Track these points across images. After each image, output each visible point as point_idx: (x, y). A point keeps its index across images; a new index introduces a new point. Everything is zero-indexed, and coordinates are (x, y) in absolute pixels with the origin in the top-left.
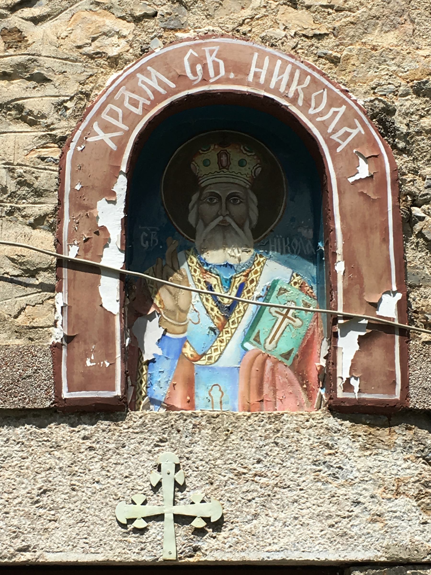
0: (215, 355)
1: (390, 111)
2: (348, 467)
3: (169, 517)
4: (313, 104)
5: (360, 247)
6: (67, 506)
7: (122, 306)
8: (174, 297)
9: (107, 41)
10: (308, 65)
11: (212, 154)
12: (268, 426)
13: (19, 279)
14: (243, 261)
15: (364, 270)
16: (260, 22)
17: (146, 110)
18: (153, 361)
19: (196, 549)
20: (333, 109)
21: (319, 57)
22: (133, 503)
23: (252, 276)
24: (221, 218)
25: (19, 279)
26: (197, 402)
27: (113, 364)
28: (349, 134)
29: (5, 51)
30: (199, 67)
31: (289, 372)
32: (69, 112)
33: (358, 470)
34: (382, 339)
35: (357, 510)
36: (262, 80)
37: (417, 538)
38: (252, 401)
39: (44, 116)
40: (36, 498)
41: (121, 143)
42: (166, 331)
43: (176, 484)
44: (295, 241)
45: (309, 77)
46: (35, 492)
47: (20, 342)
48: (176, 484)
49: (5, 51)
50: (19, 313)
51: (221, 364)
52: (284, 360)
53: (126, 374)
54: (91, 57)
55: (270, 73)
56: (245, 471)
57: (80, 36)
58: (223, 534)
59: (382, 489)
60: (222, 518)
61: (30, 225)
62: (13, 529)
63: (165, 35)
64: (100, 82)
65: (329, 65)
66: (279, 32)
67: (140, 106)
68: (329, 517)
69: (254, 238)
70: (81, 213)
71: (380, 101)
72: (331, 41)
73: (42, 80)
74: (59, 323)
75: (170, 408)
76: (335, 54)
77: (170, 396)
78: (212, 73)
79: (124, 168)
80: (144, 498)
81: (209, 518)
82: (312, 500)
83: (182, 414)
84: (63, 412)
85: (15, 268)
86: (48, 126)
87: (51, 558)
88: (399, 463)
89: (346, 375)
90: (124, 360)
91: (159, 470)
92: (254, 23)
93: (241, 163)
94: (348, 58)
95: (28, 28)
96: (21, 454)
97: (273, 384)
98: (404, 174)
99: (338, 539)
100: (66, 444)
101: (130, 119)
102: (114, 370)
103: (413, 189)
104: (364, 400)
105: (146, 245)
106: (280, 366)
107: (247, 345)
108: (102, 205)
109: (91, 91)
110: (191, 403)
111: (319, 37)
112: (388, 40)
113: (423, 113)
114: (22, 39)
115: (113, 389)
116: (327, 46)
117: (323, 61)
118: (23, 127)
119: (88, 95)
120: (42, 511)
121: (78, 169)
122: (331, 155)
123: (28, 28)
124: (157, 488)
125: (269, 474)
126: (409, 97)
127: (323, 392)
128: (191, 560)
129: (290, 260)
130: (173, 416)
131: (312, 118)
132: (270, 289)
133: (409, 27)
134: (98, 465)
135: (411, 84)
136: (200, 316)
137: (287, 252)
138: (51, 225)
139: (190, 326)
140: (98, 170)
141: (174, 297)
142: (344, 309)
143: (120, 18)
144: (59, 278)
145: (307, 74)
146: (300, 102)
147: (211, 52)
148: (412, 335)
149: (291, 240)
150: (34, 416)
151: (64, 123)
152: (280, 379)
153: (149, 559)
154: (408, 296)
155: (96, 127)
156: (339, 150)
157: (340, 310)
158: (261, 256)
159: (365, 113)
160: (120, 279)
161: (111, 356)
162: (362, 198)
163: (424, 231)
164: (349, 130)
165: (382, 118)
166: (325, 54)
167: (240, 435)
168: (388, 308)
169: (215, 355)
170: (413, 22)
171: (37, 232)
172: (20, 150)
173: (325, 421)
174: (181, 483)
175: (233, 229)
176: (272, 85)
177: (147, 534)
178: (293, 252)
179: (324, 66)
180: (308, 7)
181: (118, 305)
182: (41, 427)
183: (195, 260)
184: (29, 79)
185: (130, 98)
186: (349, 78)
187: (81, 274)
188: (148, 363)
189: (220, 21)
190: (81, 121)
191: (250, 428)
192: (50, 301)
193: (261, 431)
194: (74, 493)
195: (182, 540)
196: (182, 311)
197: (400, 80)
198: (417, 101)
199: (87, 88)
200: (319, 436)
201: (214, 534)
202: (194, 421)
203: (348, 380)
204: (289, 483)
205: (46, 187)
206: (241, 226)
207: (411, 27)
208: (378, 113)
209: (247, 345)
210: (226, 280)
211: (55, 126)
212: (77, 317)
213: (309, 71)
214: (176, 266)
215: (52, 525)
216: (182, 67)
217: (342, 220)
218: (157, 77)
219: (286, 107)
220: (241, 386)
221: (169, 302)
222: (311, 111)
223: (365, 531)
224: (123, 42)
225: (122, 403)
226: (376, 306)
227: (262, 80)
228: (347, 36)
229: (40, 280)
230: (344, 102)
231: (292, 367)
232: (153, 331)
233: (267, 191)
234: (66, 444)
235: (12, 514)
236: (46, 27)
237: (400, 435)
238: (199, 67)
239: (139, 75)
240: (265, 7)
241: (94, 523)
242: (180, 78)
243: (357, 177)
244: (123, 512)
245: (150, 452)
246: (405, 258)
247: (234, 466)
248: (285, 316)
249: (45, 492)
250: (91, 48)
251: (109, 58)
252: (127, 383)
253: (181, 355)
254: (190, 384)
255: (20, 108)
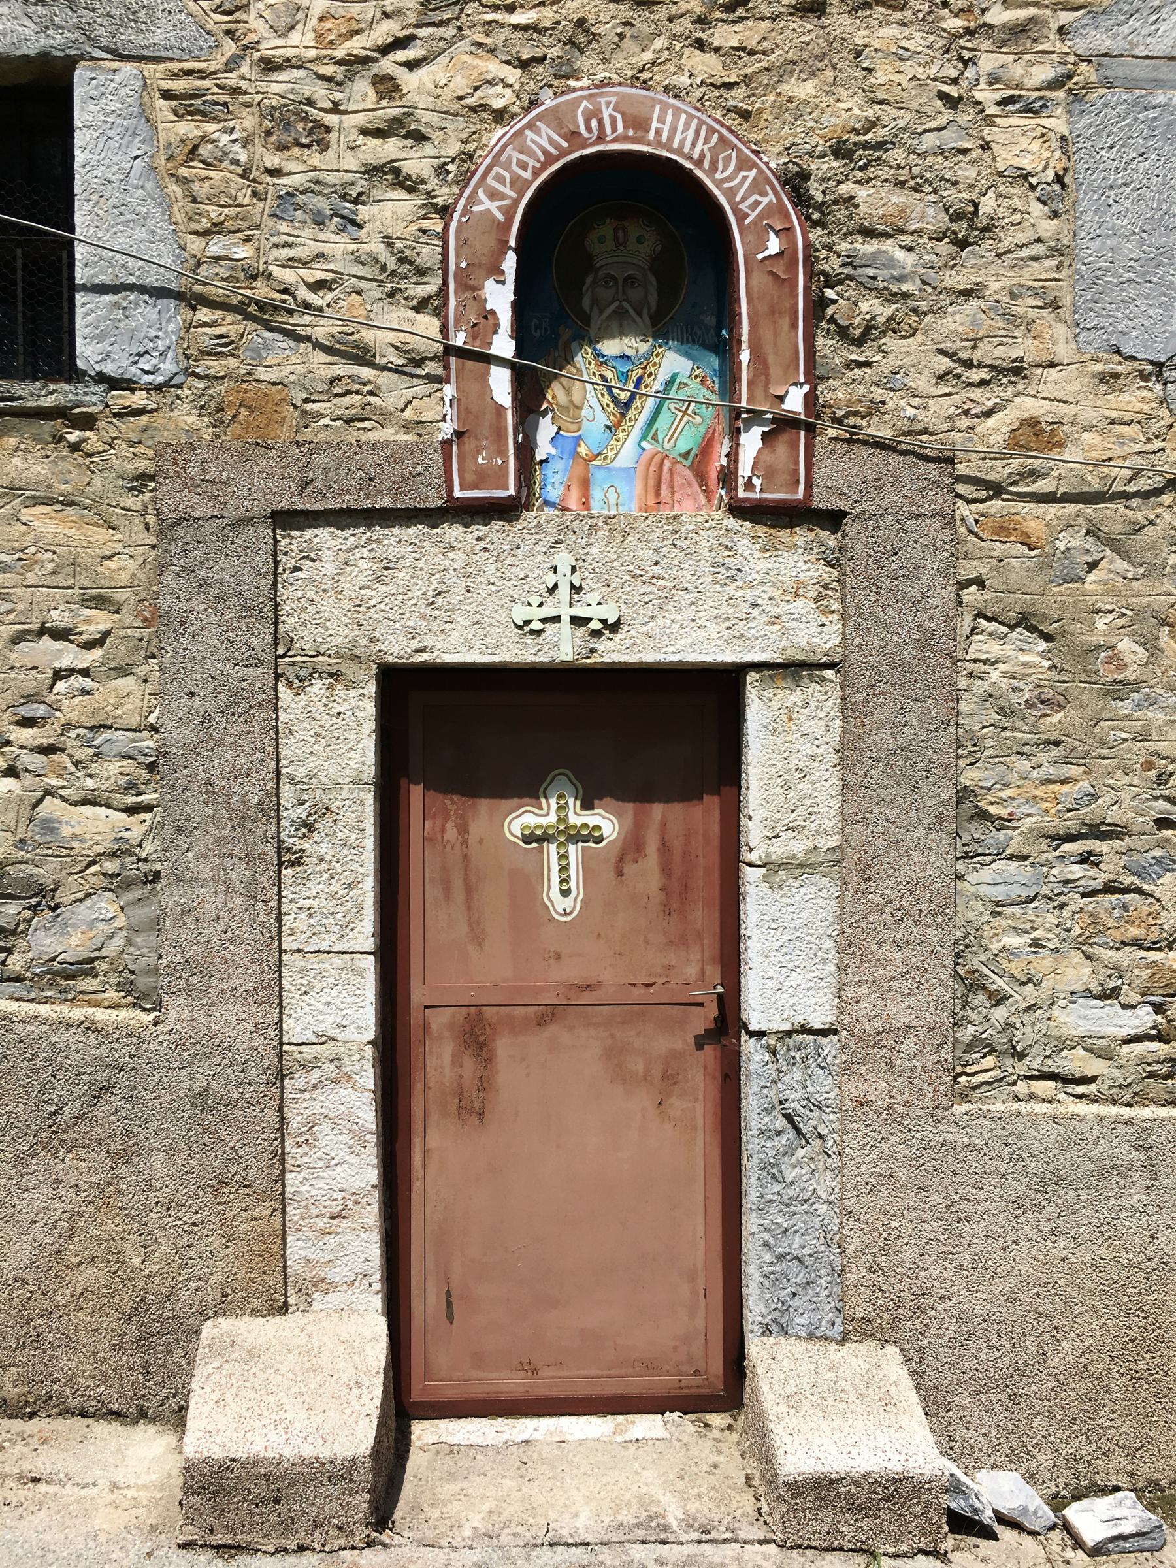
0: (611, 454)
1: (804, 176)
2: (747, 569)
3: (565, 619)
4: (720, 168)
5: (767, 335)
6: (462, 607)
7: (514, 399)
8: (568, 391)
9: (492, 91)
10: (715, 120)
11: (607, 229)
12: (666, 527)
13: (404, 369)
14: (641, 352)
15: (771, 359)
16: (663, 68)
17: (536, 173)
18: (547, 461)
19: (593, 651)
20: (743, 173)
21: (728, 110)
22: (530, 605)
23: (650, 369)
24: (616, 304)
25: (404, 369)
26: (592, 503)
27: (506, 462)
28: (759, 203)
29: (378, 102)
30: (594, 123)
31: (688, 473)
32: (451, 176)
33: (757, 572)
34: (784, 437)
35: (755, 612)
36: (664, 138)
37: (814, 640)
38: (649, 503)
39: (423, 182)
40: (431, 600)
41: (509, 213)
42: (559, 428)
43: (572, 586)
44: (696, 329)
45: (716, 135)
46: (430, 593)
47: (409, 438)
48: (572, 586)
49: (378, 102)
50: (406, 406)
51: (617, 464)
52: (682, 460)
53: (519, 472)
54: (474, 109)
55: (673, 130)
56: (642, 573)
57: (460, 85)
58: (620, 636)
59: (781, 591)
60: (619, 620)
61: (413, 308)
62: (409, 630)
63: (556, 84)
64: (484, 140)
65: (739, 120)
66: (683, 80)
67: (530, 169)
68: (727, 619)
69: (653, 326)
70: (468, 294)
71: (795, 163)
72: (741, 92)
73: (419, 137)
74: (448, 417)
75: (565, 509)
76: (745, 107)
77: (565, 497)
78: (608, 130)
79: (512, 243)
80: (540, 600)
81: (606, 620)
82: (710, 603)
83: (578, 518)
84: (456, 512)
85: (399, 356)
86: (428, 193)
87: (448, 658)
88: (799, 565)
89: (748, 473)
90: (517, 457)
91: (555, 572)
92: (655, 69)
93: (640, 240)
94: (760, 112)
95: (402, 74)
96: (414, 555)
97: (672, 486)
98: (817, 250)
99: (735, 641)
100: (460, 546)
101: (519, 185)
102: (507, 468)
103: (827, 268)
104: (766, 500)
105: (537, 334)
106: (678, 466)
107: (644, 444)
108: (490, 285)
109: (475, 151)
110: (586, 505)
111: (729, 86)
112: (804, 90)
113: (841, 178)
114: (396, 88)
115: (507, 489)
116: (737, 97)
117: (732, 115)
118: (401, 194)
119: (471, 156)
120: (437, 613)
121: (463, 243)
122: (739, 227)
123: (402, 74)
124: (553, 590)
125: (667, 576)
126: (827, 159)
127: (723, 492)
128: (588, 661)
129: (690, 351)
130: (569, 517)
131: (719, 184)
132: (669, 383)
133: (829, 74)
134: (493, 567)
135: (829, 143)
136: (595, 413)
137: (688, 342)
138: (436, 308)
139: (585, 423)
140: (484, 244)
141: (568, 391)
142: (748, 403)
143: (505, 62)
144: (446, 368)
145: (714, 131)
146: (706, 165)
147: (608, 104)
148: (818, 431)
149: (692, 329)
150: (426, 516)
151: (445, 190)
152: (678, 481)
153: (546, 660)
154: (816, 389)
155: (481, 194)
156: (747, 221)
157: (744, 404)
158: (660, 347)
159: (778, 178)
160: (512, 370)
161: (503, 453)
162: (770, 277)
163: (836, 316)
164: (759, 198)
165: (795, 183)
166: (735, 107)
167: (637, 536)
168: (795, 402)
169: (611, 454)
170: (834, 68)
171: (421, 315)
172: (399, 222)
173: (725, 522)
174: (577, 585)
175: (631, 316)
176: (676, 145)
177: (543, 636)
178: (694, 342)
179: (733, 121)
180: (717, 50)
181: (509, 398)
182: (433, 527)
183: (589, 351)
184: (405, 137)
185: (518, 160)
186: (760, 136)
187: (469, 364)
188: (541, 462)
189: (618, 66)
190: (465, 187)
191: (647, 530)
192: (438, 394)
193: (659, 533)
194: (469, 595)
195: (579, 642)
196: (577, 407)
197: (817, 139)
198: (835, 164)
199: (471, 147)
200: (718, 538)
201: (611, 636)
202: (590, 522)
203: (750, 478)
204: (686, 585)
205: (428, 265)
206: (639, 314)
207: (832, 74)
208: (791, 178)
209: (644, 444)
210: (623, 373)
211: (436, 193)
212: (468, 411)
213: (717, 127)
214: (569, 358)
215: (448, 626)
216: (576, 122)
217: (748, 303)
218: (548, 135)
219: (691, 170)
220: (638, 487)
221: (562, 398)
222: (718, 176)
223: (762, 633)
224: (508, 91)
225: (515, 502)
226: (781, 399)
227: (664, 138)
228: (760, 85)
229: (427, 370)
230: (755, 165)
231: (691, 467)
232: (546, 429)
233: (666, 270)
234: (460, 546)
235: (408, 615)
236: (423, 72)
237: (801, 536)
238: (594, 123)
239: (527, 132)
240: (668, 49)
241: (491, 625)
242: (573, 136)
243: (766, 254)
244: (520, 614)
245: (545, 553)
246: (814, 346)
247: (631, 568)
248: (685, 413)
249: (440, 593)
250: (473, 99)
251: (494, 111)
252: (520, 482)
253: (575, 454)
254: (585, 484)
255: (397, 172)
